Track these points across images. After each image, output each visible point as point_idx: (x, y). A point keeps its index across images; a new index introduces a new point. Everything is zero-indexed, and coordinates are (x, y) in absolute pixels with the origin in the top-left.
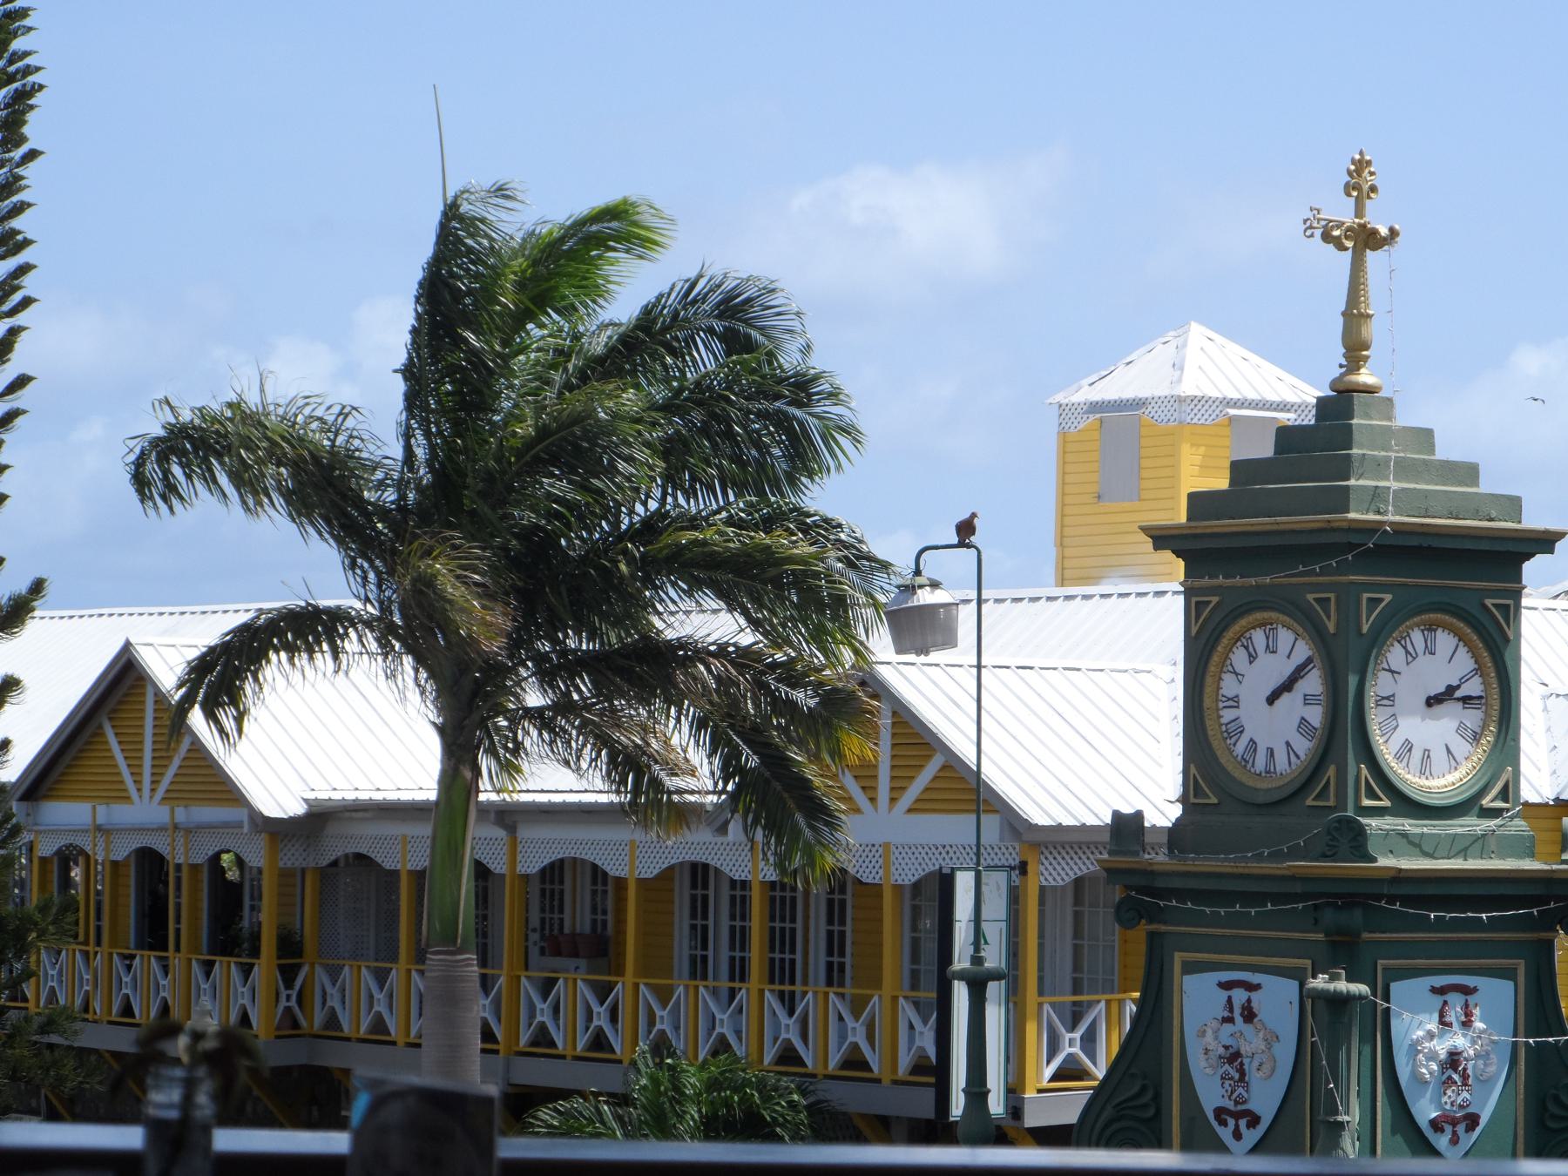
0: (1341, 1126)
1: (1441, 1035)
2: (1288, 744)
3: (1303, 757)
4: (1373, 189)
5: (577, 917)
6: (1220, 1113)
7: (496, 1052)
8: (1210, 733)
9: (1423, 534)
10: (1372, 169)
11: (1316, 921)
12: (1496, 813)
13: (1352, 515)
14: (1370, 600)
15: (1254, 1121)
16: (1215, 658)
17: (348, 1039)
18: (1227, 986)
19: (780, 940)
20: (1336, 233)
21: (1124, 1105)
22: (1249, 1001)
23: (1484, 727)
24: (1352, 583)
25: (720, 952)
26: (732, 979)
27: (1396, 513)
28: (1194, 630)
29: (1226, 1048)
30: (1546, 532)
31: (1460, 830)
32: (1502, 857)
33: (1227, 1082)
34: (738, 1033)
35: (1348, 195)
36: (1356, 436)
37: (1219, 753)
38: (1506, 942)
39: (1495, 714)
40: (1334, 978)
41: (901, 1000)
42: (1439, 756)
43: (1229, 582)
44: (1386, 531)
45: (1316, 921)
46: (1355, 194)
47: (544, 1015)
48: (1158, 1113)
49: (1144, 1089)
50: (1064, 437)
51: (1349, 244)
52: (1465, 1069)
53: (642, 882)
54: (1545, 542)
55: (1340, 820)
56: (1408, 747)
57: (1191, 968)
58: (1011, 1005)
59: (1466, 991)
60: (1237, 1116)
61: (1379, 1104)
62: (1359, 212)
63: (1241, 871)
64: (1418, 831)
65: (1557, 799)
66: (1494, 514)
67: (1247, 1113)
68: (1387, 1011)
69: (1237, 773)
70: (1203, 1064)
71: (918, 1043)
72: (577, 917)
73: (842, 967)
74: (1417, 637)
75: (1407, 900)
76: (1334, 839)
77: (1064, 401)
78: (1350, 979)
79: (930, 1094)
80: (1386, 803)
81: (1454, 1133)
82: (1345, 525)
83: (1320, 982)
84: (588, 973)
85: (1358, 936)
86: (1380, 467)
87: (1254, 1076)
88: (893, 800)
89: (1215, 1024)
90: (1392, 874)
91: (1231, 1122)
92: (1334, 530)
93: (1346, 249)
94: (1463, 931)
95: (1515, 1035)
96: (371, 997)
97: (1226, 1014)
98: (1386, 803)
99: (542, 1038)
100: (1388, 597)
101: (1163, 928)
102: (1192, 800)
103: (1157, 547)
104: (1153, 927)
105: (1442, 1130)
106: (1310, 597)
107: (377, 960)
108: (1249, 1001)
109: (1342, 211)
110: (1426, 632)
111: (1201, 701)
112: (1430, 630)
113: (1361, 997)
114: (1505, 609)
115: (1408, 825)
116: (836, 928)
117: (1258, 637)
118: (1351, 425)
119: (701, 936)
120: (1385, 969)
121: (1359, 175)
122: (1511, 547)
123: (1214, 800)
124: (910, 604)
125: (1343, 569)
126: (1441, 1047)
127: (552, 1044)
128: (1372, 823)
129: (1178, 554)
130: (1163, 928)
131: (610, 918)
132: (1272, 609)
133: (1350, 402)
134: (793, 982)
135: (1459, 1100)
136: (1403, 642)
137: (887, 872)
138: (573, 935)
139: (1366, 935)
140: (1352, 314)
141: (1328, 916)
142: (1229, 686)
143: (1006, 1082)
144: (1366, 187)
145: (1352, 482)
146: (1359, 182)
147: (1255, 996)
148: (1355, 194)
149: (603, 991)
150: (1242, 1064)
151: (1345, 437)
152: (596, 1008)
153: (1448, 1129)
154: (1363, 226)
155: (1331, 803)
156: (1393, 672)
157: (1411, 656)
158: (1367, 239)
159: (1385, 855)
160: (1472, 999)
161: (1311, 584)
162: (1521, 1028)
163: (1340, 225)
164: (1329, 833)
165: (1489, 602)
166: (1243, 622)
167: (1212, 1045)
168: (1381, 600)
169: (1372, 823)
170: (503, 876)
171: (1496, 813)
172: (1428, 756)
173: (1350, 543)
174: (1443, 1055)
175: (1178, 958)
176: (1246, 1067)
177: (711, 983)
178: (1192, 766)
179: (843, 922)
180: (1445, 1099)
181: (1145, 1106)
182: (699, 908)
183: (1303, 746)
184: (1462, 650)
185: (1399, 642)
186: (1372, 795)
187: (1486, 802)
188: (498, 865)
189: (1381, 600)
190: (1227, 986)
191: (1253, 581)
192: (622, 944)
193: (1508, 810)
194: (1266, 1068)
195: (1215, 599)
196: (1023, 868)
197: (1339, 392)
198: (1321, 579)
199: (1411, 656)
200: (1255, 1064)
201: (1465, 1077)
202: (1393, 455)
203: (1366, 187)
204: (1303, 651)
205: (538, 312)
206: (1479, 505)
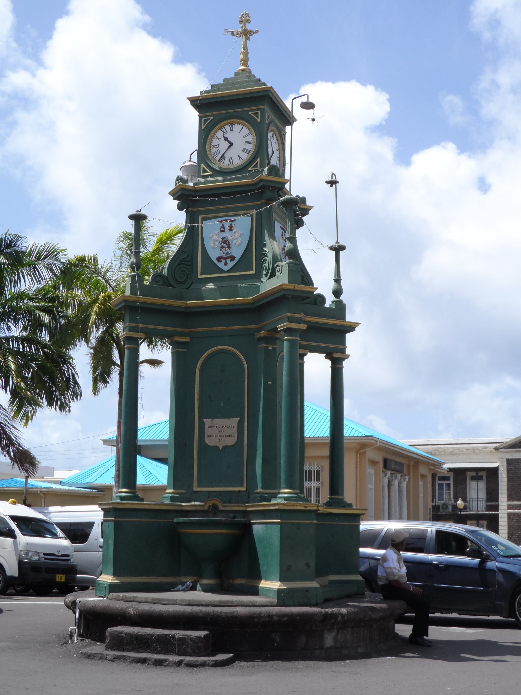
21: (183, 262)
48: (192, 264)
49: (188, 256)
98: (210, 173)
101: (194, 210)
110: (231, 126)
112: (232, 125)
136: (222, 130)
156: (218, 138)
160: (233, 223)
172: (232, 159)
181: (188, 261)
185: (221, 130)
205: (116, 519)
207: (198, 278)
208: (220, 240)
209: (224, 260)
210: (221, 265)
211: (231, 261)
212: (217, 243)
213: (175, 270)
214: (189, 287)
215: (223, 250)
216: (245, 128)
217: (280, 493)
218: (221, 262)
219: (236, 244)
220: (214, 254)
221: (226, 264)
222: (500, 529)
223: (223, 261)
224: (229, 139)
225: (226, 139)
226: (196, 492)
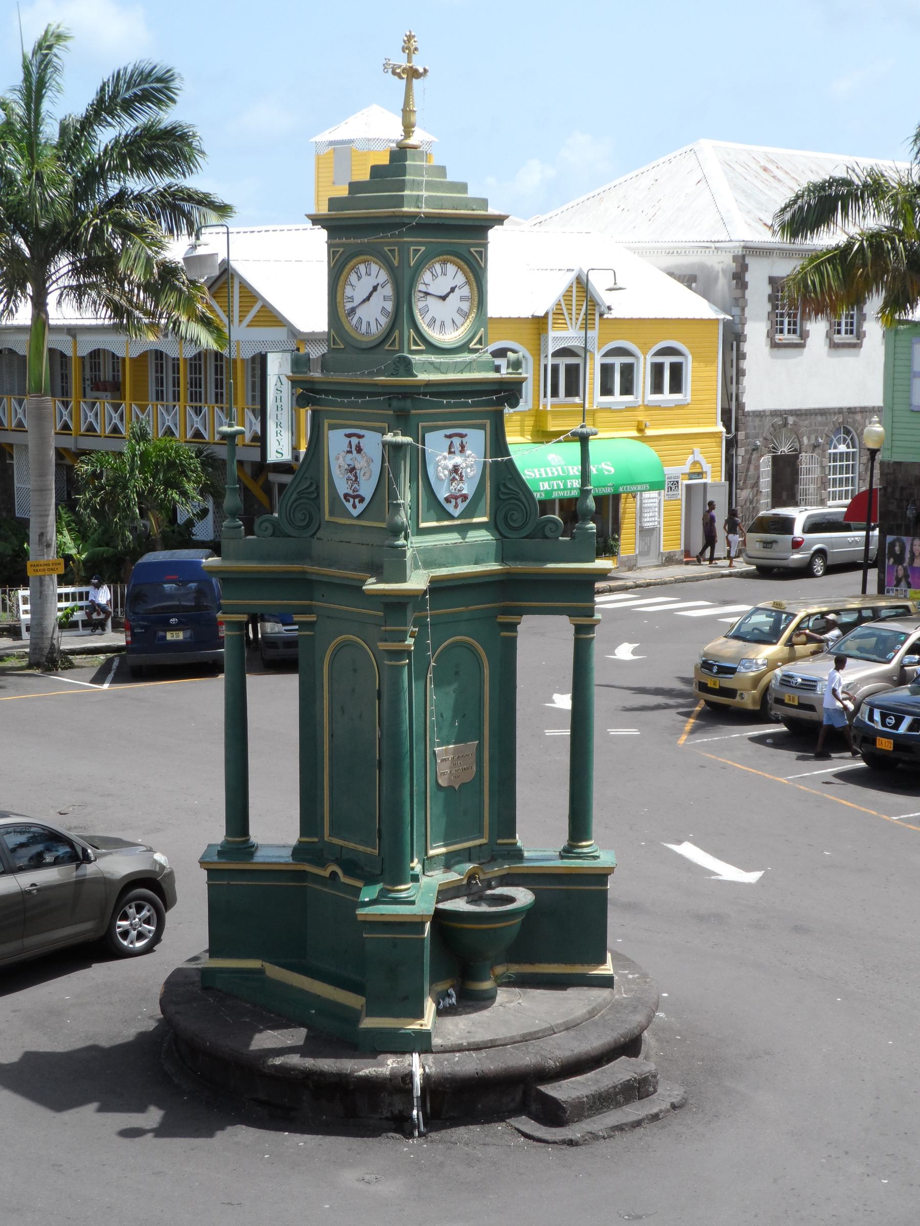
0: (399, 505)
1: (450, 459)
2: (376, 320)
3: (383, 326)
4: (416, 49)
5: (106, 374)
6: (346, 496)
7: (71, 434)
8: (340, 314)
9: (439, 218)
10: (416, 39)
11: (390, 405)
12: (476, 351)
13: (405, 209)
14: (414, 250)
15: (362, 500)
16: (342, 278)
17: (7, 430)
18: (349, 436)
19: (195, 383)
20: (398, 71)
22: (359, 443)
23: (471, 309)
24: (406, 242)
25: (169, 389)
26: (174, 400)
27: (426, 207)
28: (332, 265)
29: (349, 465)
30: (500, 216)
31: (459, 360)
32: (479, 371)
33: (349, 482)
34: (175, 425)
35: (404, 51)
36: (408, 170)
37: (344, 324)
38: (481, 412)
39: (476, 303)
40: (395, 435)
41: (246, 409)
42: (448, 323)
43: (348, 241)
44: (421, 217)
45: (390, 405)
46: (407, 51)
47: (91, 419)
48: (318, 497)
49: (311, 484)
50: (318, 157)
51: (405, 76)
52: (461, 473)
53: (132, 359)
54: (499, 220)
55: (400, 357)
56: (433, 320)
57: (332, 427)
58: (294, 411)
59: (462, 436)
60: (354, 497)
61: (420, 491)
62: (409, 60)
63: (354, 381)
64: (438, 360)
65: (533, 316)
66: (474, 207)
67: (358, 496)
68: (424, 451)
69: (353, 334)
70: (338, 472)
71: (254, 428)
72: (106, 374)
73: (222, 394)
74: (438, 267)
75: (433, 395)
76: (397, 366)
77: (318, 141)
78: (403, 435)
79: (258, 451)
80: (423, 347)
81: (456, 503)
82: (401, 214)
83: (389, 437)
84: (112, 399)
85: (409, 412)
86: (416, 185)
87: (362, 479)
88: (240, 321)
89: (343, 454)
90: (425, 383)
91: (352, 500)
92: (396, 216)
93: (403, 78)
94: (460, 408)
95: (485, 458)
96: (16, 411)
97: (349, 449)
98: (423, 347)
99: (91, 428)
100: (423, 249)
101: (319, 408)
102: (483, 249)
103: (314, 224)
104: (315, 407)
105: (451, 502)
106: (386, 249)
107: (19, 395)
108: (359, 443)
109: (401, 60)
111: (336, 299)
112: (444, 264)
113: (408, 444)
114: (480, 253)
115: (433, 358)
116: (219, 377)
117: (362, 268)
118: (405, 165)
119: (160, 382)
120: (423, 427)
121: (409, 42)
122: (483, 223)
123: (342, 347)
124: (194, 254)
125: (401, 235)
126: (450, 464)
127: (95, 431)
128: (415, 358)
129: (323, 227)
130: (319, 408)
131: (120, 374)
132: (368, 254)
133: (406, 153)
134: (200, 401)
135: (458, 488)
137: (238, 353)
138: (105, 382)
139: (413, 412)
140: (406, 111)
141: (395, 403)
142: (349, 291)
143: (292, 445)
144: (412, 48)
145: (407, 193)
146: (409, 47)
147: (361, 440)
148: (407, 51)
149: (116, 407)
150: (356, 473)
151: (403, 171)
152: (114, 415)
153: (453, 501)
154: (411, 67)
155: (397, 348)
156: (426, 284)
157: (435, 276)
158: (413, 74)
159: (422, 373)
160: (465, 440)
161: (386, 242)
162: (488, 454)
163: (400, 67)
164: (394, 364)
165: (472, 250)
166: (354, 261)
167: (342, 464)
168: (420, 250)
169: (415, 358)
170: (71, 357)
171: (476, 351)
173: (404, 223)
174: (451, 467)
175: (326, 423)
176: (358, 474)
177: (165, 403)
178: (332, 330)
179: (222, 374)
180: (452, 487)
181: (312, 492)
182: (160, 369)
183: (384, 321)
184: (460, 273)
186: (416, 344)
187: (471, 346)
188: (69, 352)
189: (420, 250)
190: (349, 436)
191: (359, 241)
192: (125, 385)
193: (482, 349)
194: (367, 475)
195: (341, 250)
196: (298, 349)
197: (401, 148)
198: (391, 240)
199: (435, 276)
200: (362, 473)
201: (461, 477)
202: (424, 179)
203: (412, 48)
204: (383, 276)
206: (467, 203)
211: (462, 502)
218: (451, 502)
220: (342, 487)
224: (451, 294)
225: (452, 290)
226: (432, 857)
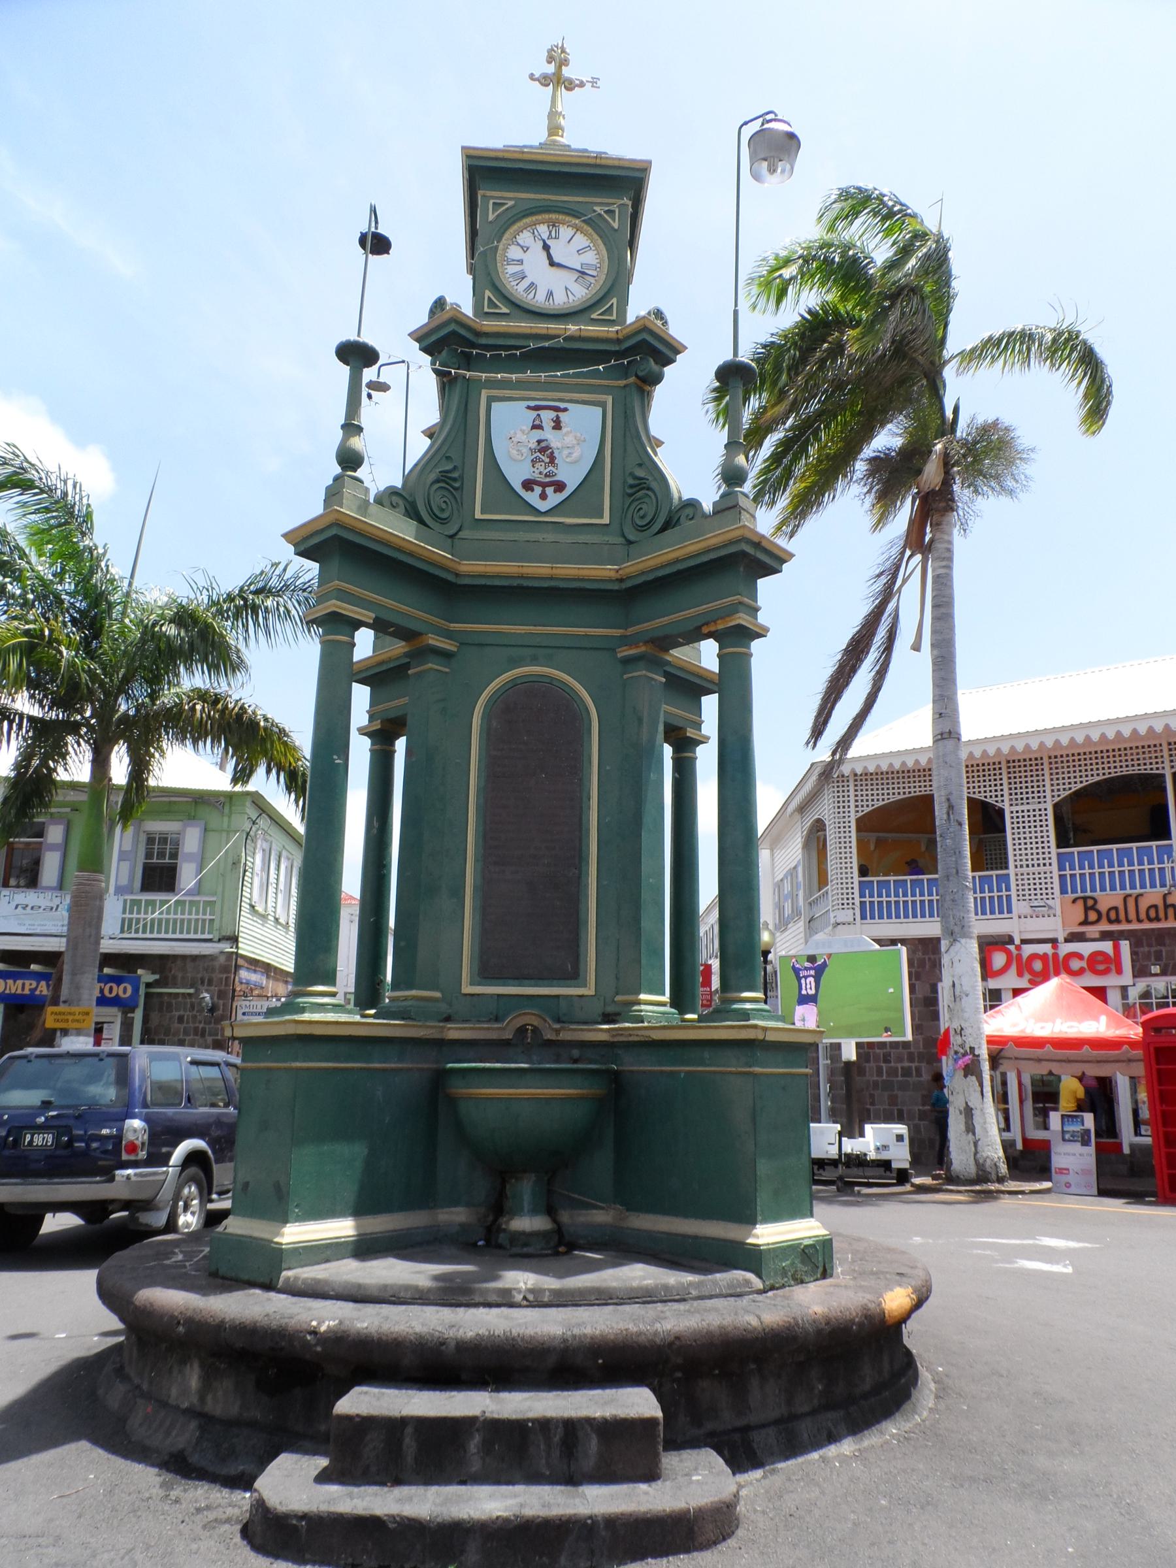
49: (455, 468)
98: (505, 310)
112: (554, 226)
181: (455, 480)
207: (476, 517)
208: (533, 444)
209: (541, 489)
210: (533, 498)
211: (555, 491)
212: (525, 451)
213: (429, 494)
214: (456, 534)
215: (537, 465)
216: (579, 236)
217: (639, 1003)
218: (533, 490)
219: (568, 460)
221: (543, 496)
222: (358, 908)
223: (538, 490)
